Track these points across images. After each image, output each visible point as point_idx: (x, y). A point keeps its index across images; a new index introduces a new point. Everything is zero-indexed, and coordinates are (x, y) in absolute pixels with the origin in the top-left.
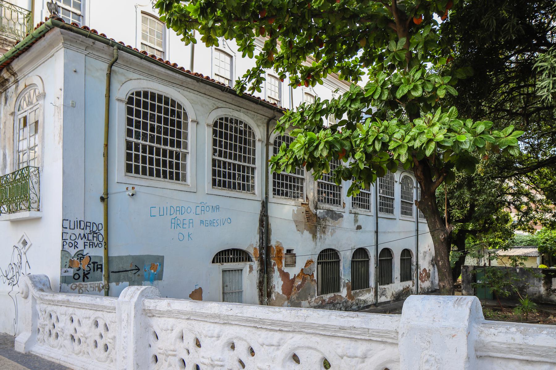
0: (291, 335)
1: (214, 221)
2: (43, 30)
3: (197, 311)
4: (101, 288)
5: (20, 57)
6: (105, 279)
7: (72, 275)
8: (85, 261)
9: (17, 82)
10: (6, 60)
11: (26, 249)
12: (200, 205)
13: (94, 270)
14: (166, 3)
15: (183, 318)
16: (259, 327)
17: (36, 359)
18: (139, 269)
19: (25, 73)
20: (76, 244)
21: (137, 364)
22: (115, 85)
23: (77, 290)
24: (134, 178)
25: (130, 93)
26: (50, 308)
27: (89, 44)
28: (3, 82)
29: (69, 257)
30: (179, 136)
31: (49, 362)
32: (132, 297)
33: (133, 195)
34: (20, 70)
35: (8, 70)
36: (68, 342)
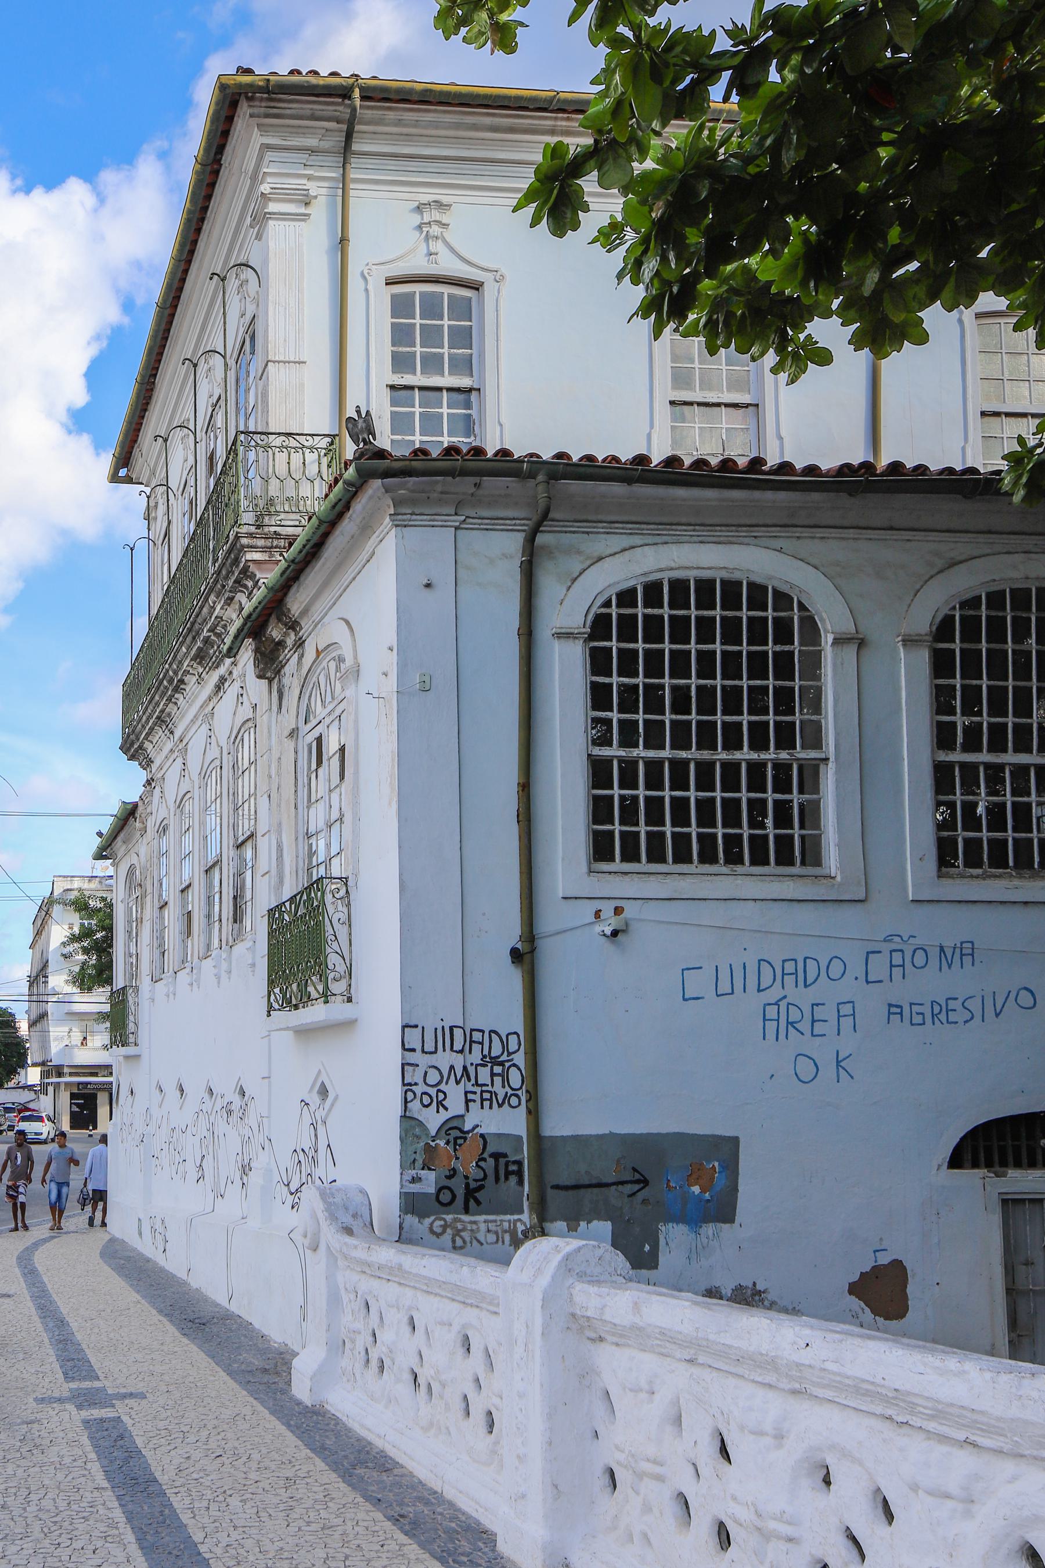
0: (1009, 1467)
1: (952, 1004)
2: (340, 497)
3: (712, 1337)
4: (520, 1235)
5: (302, 578)
6: (531, 1209)
7: (432, 1190)
8: (470, 1151)
9: (300, 644)
10: (270, 595)
11: (326, 1110)
12: (886, 947)
13: (497, 1179)
14: (671, 292)
15: (678, 1356)
16: (900, 1419)
17: (331, 1426)
18: (645, 1182)
19: (316, 617)
20: (441, 1096)
21: (556, 1486)
22: (549, 587)
23: (447, 1237)
24: (618, 879)
25: (599, 601)
26: (367, 1285)
27: (464, 494)
28: (272, 651)
29: (424, 1137)
30: (785, 700)
31: (359, 1439)
32: (539, 1271)
33: (615, 933)
34: (305, 612)
35: (279, 620)
36: (404, 1388)
